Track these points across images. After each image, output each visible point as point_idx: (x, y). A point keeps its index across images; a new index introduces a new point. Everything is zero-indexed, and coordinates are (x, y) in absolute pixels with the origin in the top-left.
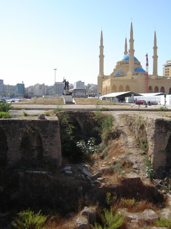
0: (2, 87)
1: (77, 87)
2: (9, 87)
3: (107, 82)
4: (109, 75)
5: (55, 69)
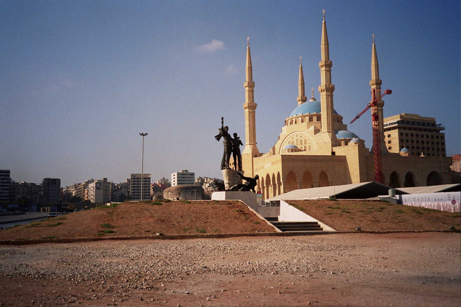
0: (7, 186)
1: (178, 184)
2: (25, 186)
3: (270, 164)
4: (344, 123)
5: (143, 135)
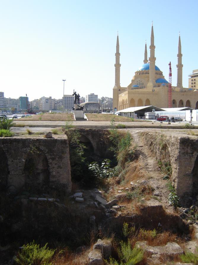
0: (3, 100)
1: (89, 101)
2: (11, 100)
3: (124, 95)
4: (127, 87)
5: (63, 80)
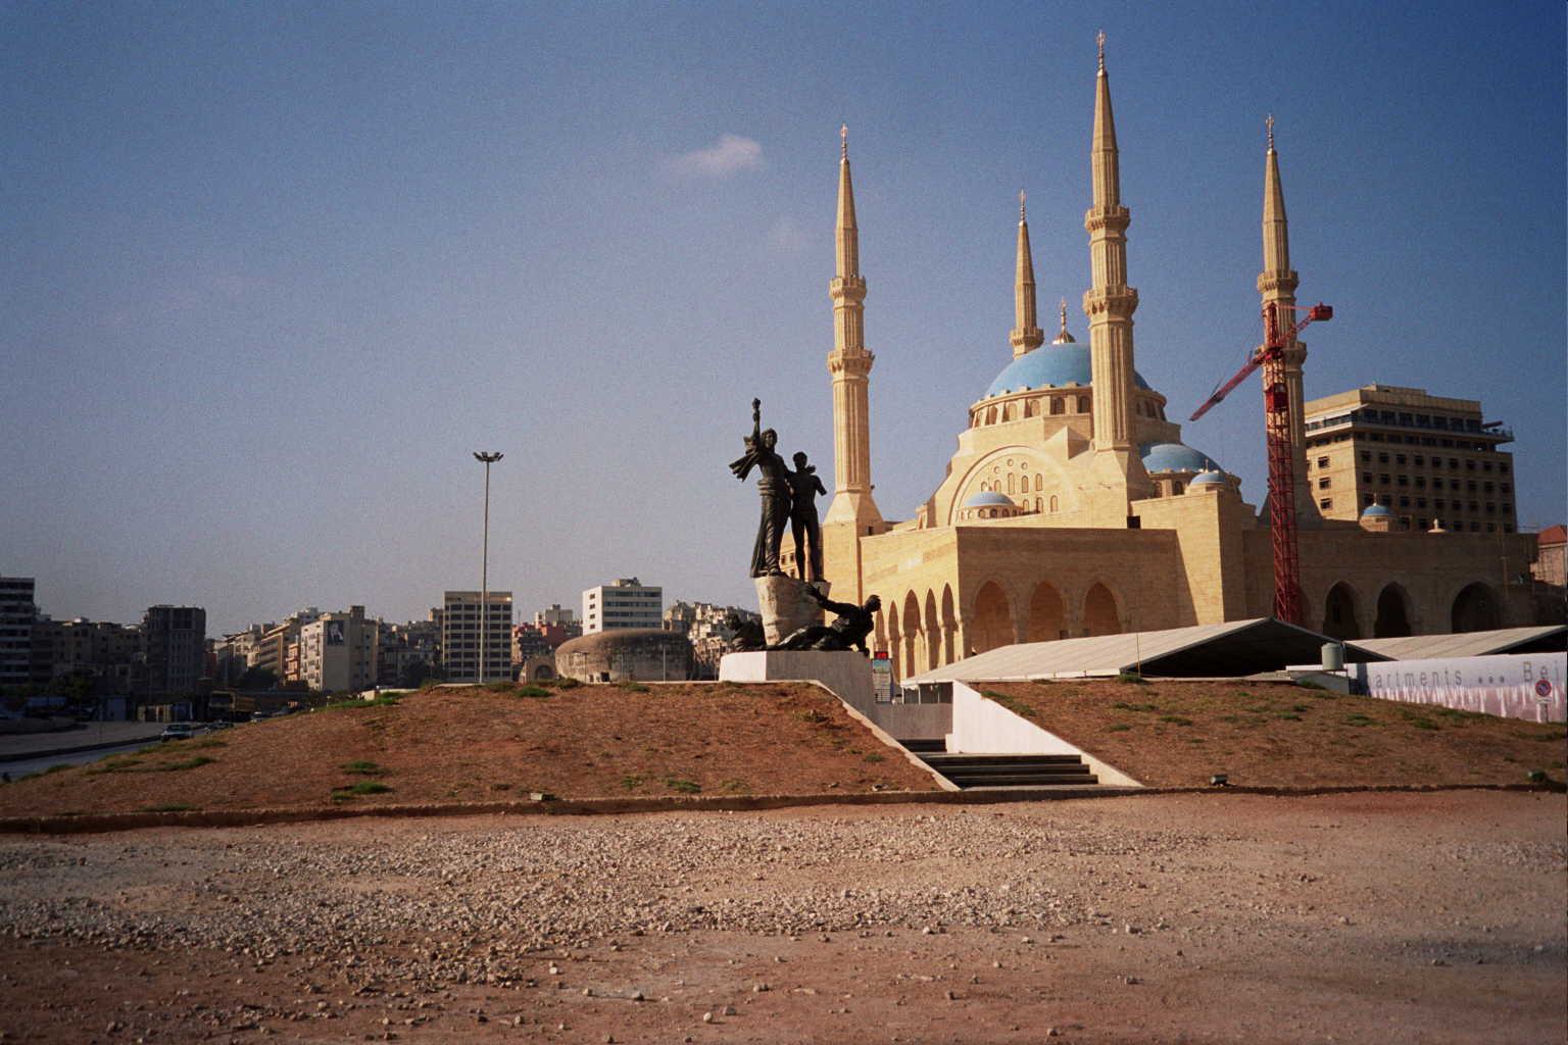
0: (25, 633)
1: (606, 625)
2: (85, 633)
3: (918, 559)
4: (1169, 420)
5: (485, 458)
